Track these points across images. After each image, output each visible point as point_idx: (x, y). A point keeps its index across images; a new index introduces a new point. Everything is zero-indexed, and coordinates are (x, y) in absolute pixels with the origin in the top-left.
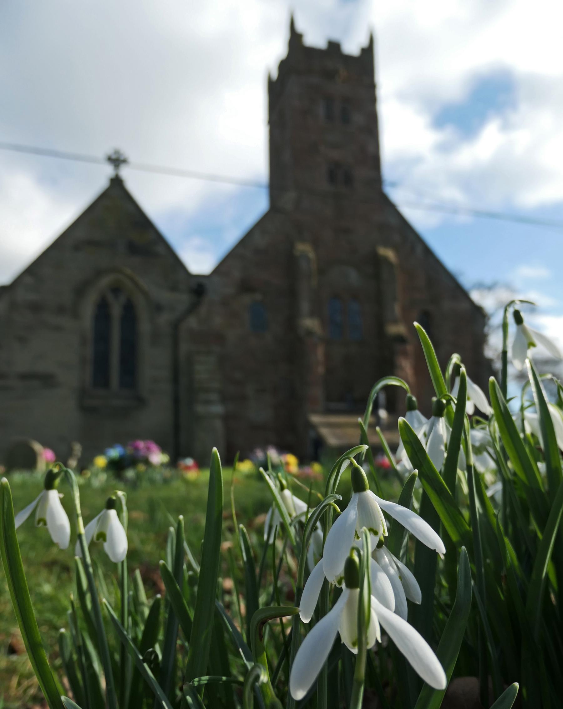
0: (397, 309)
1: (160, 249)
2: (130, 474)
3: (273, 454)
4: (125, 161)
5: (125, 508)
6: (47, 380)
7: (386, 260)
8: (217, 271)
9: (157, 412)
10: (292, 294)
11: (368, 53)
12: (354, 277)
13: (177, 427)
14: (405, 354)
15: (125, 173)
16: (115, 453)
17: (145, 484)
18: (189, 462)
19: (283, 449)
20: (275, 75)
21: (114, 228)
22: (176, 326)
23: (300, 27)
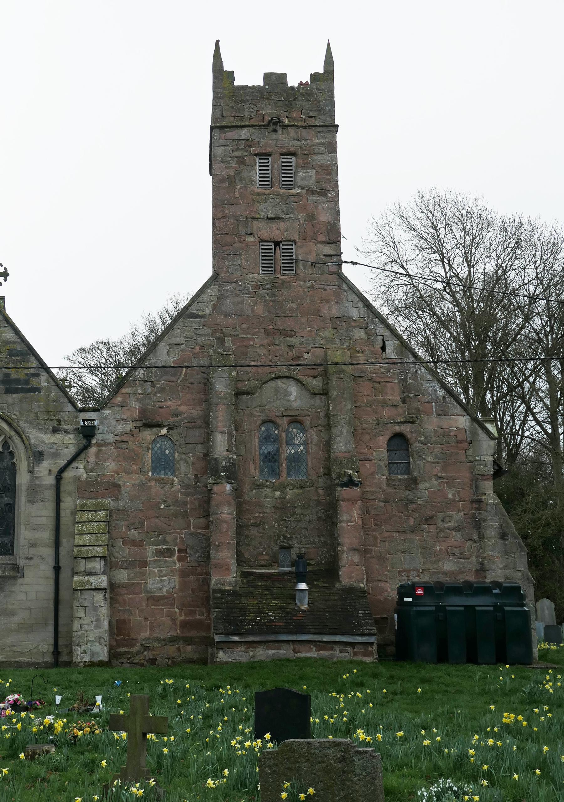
10: (206, 424)
11: (324, 80)
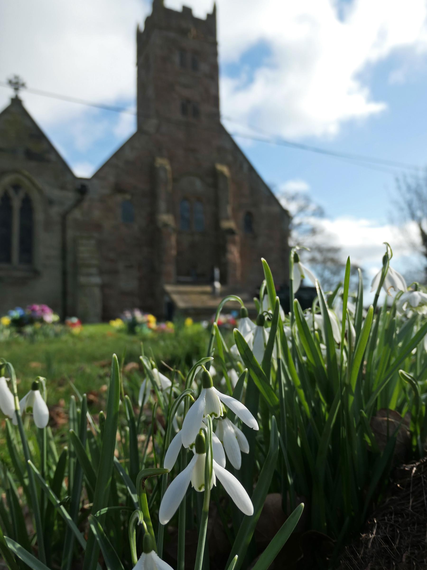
0: (229, 210)
1: (52, 157)
2: (29, 329)
3: (139, 315)
4: (23, 85)
5: (45, 388)
7: (222, 174)
8: (96, 176)
9: (49, 281)
10: (153, 196)
11: (212, 17)
12: (198, 185)
13: (65, 293)
14: (234, 242)
15: (23, 95)
16: (16, 314)
17: (40, 338)
18: (75, 320)
19: (145, 310)
20: (142, 27)
22: (64, 217)
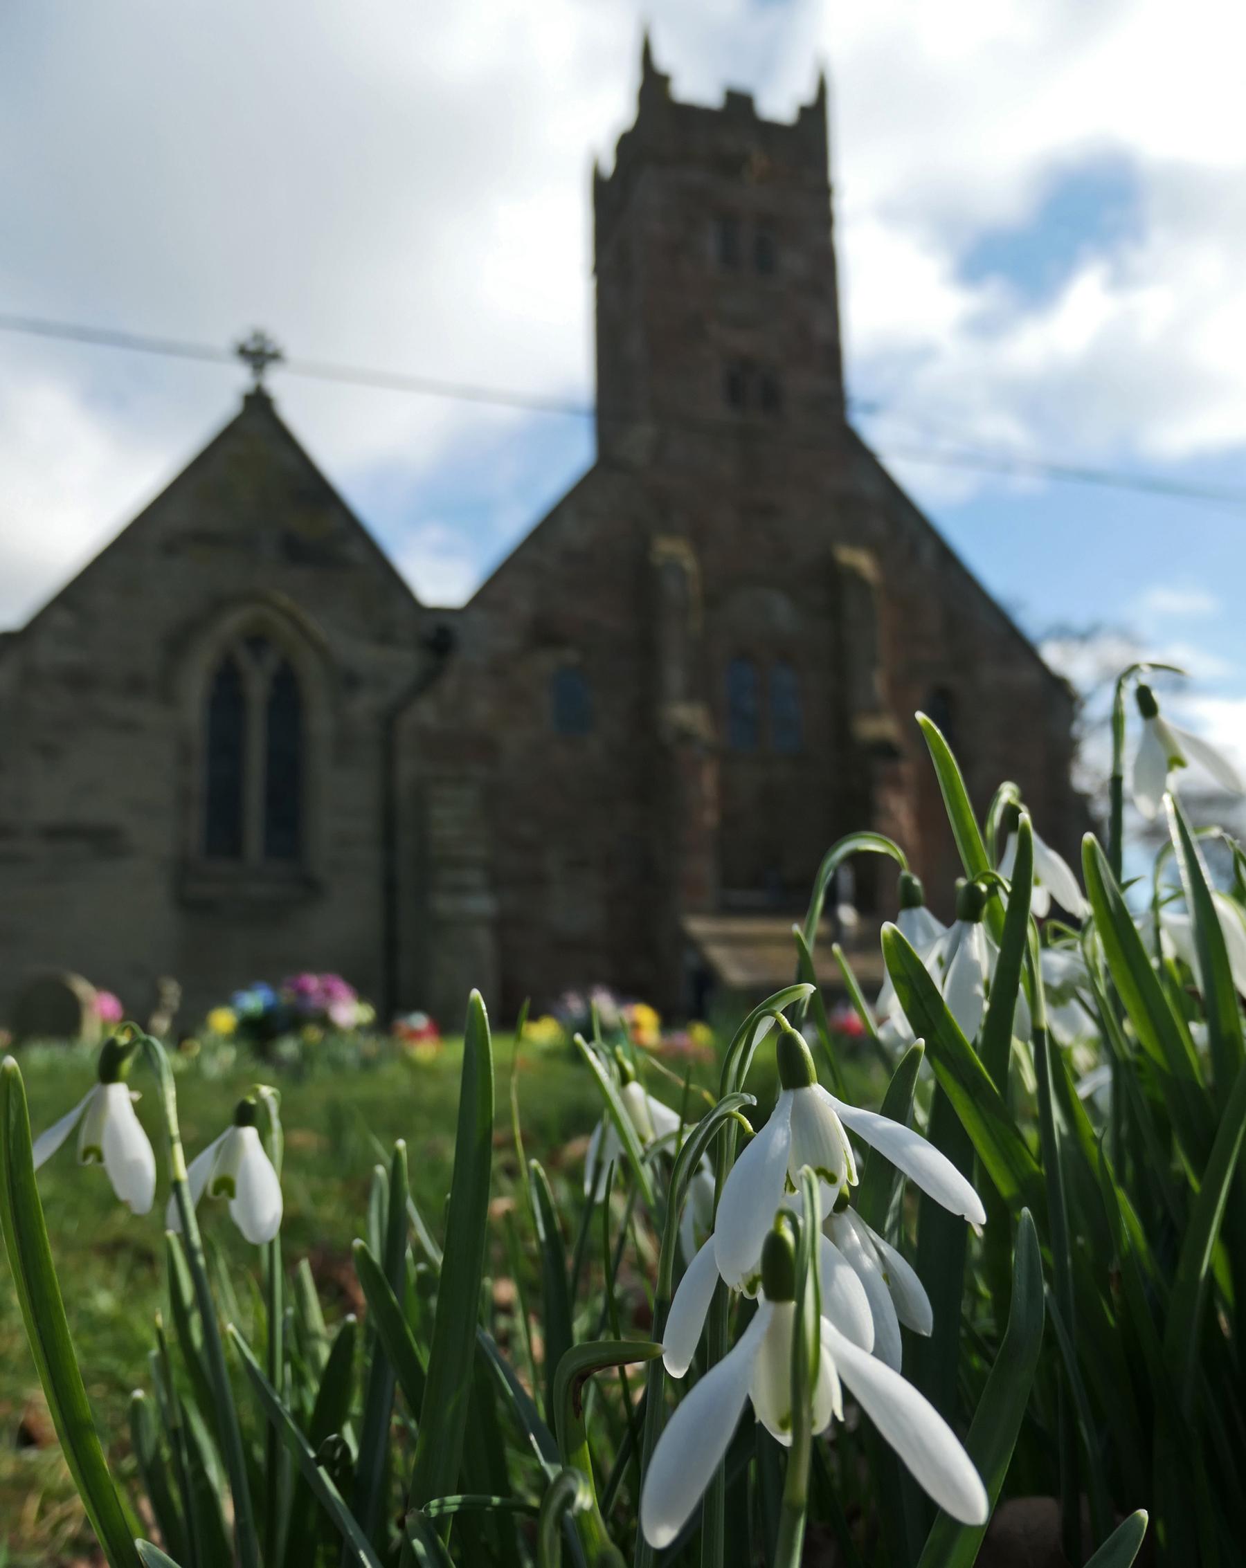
0: (879, 683)
1: (354, 551)
2: (288, 1047)
3: (604, 1005)
4: (276, 357)
5: (276, 1124)
6: (105, 841)
7: (853, 575)
8: (480, 599)
9: (348, 912)
10: (646, 650)
11: (814, 116)
12: (782, 612)
13: (391, 944)
14: (896, 783)
15: (278, 383)
16: (254, 1001)
17: (320, 1070)
18: (419, 1021)
19: (626, 993)
20: (608, 165)
21: (253, 504)
22: (389, 721)
23: (665, 59)
